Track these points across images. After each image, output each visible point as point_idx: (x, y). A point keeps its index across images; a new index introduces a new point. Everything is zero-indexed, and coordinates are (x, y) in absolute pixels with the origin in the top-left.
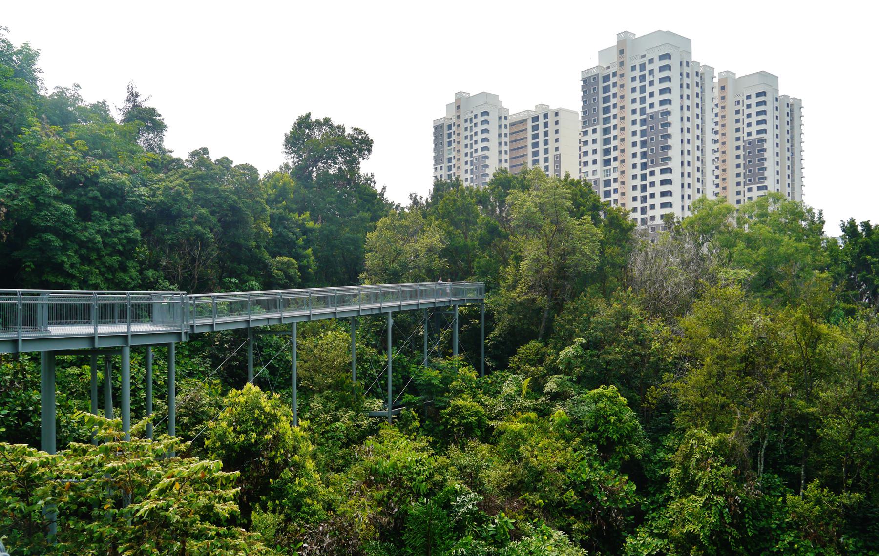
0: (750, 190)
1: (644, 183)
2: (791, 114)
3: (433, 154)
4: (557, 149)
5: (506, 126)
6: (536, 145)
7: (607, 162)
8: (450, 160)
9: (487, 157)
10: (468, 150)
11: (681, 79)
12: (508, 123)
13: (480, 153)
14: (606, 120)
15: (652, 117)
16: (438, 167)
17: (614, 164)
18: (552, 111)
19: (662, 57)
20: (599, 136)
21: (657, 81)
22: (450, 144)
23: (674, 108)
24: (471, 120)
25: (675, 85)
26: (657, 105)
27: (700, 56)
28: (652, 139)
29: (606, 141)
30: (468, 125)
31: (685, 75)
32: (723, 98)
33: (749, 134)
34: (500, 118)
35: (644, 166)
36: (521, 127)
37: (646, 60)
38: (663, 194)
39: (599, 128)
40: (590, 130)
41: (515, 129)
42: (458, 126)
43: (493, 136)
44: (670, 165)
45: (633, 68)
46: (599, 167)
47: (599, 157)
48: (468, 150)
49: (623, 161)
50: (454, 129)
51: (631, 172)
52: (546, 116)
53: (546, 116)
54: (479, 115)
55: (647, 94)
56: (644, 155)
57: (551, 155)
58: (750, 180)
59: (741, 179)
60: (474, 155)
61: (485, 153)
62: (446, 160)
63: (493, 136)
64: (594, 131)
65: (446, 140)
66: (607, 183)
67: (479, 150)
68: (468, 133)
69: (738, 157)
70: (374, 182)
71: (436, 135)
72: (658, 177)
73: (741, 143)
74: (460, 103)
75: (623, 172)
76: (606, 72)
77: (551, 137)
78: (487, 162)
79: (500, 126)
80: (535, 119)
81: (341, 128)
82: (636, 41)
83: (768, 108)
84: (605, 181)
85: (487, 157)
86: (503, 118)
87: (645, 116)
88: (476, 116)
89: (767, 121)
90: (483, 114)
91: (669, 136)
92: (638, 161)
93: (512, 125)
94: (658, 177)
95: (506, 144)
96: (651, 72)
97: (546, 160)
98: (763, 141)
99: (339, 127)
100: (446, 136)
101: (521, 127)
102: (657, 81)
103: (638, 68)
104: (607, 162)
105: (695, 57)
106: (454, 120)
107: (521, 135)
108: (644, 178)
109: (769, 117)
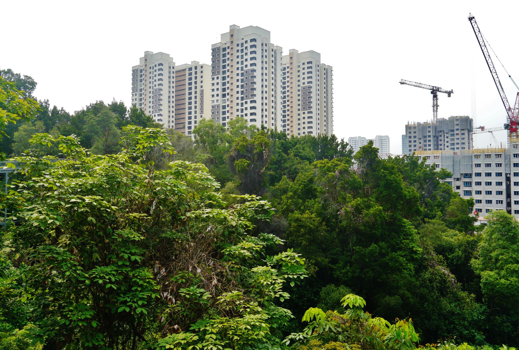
0: (304, 113)
1: (242, 108)
2: (326, 74)
3: (132, 86)
4: (202, 87)
5: (173, 72)
6: (190, 84)
7: (224, 96)
8: (141, 90)
9: (161, 90)
10: (239, 66)
11: (262, 53)
12: (174, 70)
13: (157, 87)
14: (224, 72)
15: (246, 72)
16: (134, 94)
17: (227, 97)
18: (200, 65)
19: (252, 40)
20: (220, 81)
21: (249, 53)
22: (141, 81)
23: (258, 68)
24: (153, 67)
25: (258, 56)
26: (249, 66)
27: (275, 40)
28: (246, 84)
29: (224, 84)
30: (151, 70)
31: (264, 51)
32: (291, 63)
33: (304, 83)
34: (170, 67)
35: (242, 98)
36: (183, 73)
37: (244, 41)
38: (252, 114)
39: (220, 76)
40: (215, 77)
41: (179, 74)
42: (146, 71)
43: (165, 77)
44: (255, 99)
45: (238, 45)
46: (220, 98)
47: (220, 92)
48: (151, 85)
49: (232, 96)
50: (143, 72)
51: (236, 101)
52: (196, 68)
53: (196, 68)
54: (157, 65)
55: (244, 60)
56: (242, 93)
57: (199, 90)
58: (304, 108)
59: (300, 107)
60: (154, 88)
61: (160, 87)
62: (139, 90)
63: (165, 77)
64: (218, 78)
65: (139, 78)
66: (224, 107)
67: (157, 85)
68: (151, 75)
69: (299, 95)
70: (49, 105)
71: (133, 75)
72: (249, 105)
73: (300, 88)
74: (148, 57)
75: (232, 101)
76: (224, 46)
77: (199, 80)
78: (161, 92)
79: (170, 72)
80: (190, 69)
81: (18, 75)
82: (239, 30)
83: (313, 70)
84: (223, 106)
85: (161, 90)
86: (172, 68)
87: (243, 72)
88: (156, 66)
89: (313, 78)
90: (159, 65)
91: (255, 83)
92: (240, 95)
93: (179, 71)
94: (249, 105)
95: (173, 82)
96: (246, 48)
97: (196, 92)
98: (311, 87)
99: (17, 74)
100: (139, 76)
101: (183, 73)
102: (249, 53)
103: (240, 45)
104: (224, 96)
105: (272, 42)
106: (144, 67)
107: (182, 78)
108: (242, 105)
109: (313, 75)
